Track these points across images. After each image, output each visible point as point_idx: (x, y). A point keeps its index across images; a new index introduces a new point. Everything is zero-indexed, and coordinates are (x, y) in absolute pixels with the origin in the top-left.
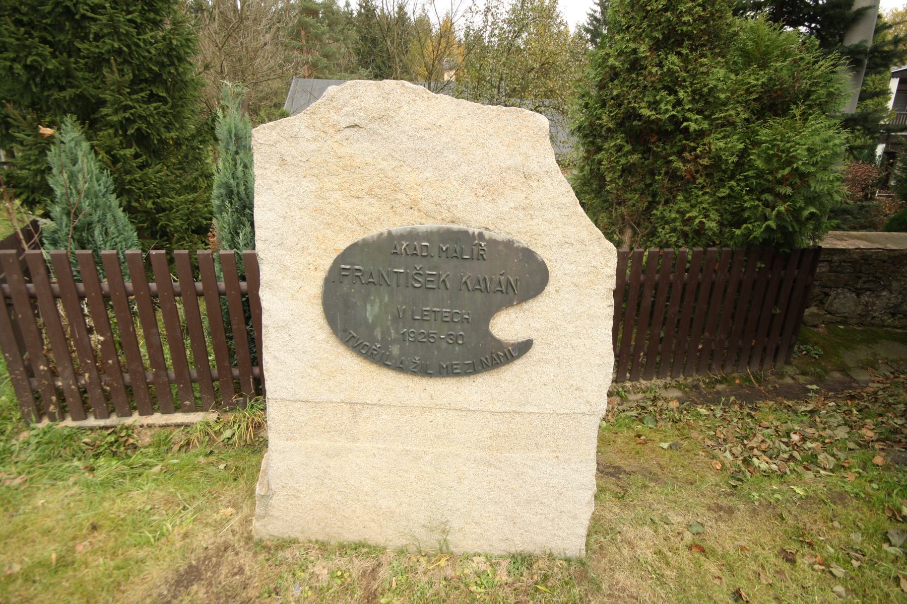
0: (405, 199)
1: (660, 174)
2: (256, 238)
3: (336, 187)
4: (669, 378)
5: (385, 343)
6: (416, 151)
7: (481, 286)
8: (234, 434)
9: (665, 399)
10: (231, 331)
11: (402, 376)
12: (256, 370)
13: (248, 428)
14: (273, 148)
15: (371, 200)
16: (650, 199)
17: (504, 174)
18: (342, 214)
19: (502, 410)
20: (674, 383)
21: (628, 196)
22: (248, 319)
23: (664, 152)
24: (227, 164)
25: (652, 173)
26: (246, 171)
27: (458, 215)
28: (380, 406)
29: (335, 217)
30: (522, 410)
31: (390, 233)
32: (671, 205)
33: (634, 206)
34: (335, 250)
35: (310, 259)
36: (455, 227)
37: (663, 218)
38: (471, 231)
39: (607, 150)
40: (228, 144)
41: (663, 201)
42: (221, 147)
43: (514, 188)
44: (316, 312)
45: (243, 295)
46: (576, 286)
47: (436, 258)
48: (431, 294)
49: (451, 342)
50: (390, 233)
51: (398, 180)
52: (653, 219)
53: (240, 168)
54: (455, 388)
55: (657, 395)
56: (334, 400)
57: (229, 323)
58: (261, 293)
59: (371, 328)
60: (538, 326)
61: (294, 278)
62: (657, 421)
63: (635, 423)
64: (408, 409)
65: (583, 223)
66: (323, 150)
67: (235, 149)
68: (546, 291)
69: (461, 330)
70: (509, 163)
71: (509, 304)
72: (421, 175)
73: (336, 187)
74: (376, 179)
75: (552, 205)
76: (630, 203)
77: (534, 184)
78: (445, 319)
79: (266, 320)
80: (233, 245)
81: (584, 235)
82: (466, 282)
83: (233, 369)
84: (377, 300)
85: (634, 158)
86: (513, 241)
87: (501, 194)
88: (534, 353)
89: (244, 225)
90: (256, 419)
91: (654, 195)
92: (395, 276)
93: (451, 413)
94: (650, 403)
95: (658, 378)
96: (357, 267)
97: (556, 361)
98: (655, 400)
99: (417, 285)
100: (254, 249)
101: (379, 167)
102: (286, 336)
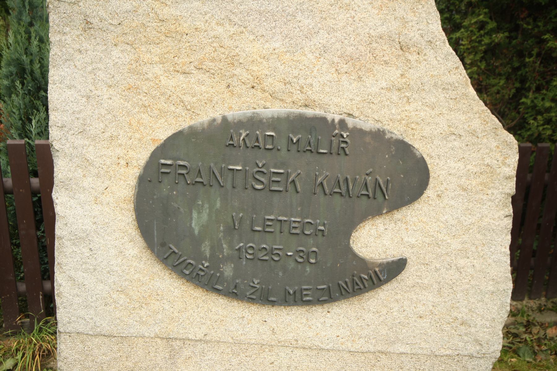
0: (245, 76)
1: (530, 56)
2: (50, 123)
3: (156, 59)
4: (543, 299)
5: (216, 261)
6: (260, 14)
7: (342, 189)
8: (16, 365)
9: (542, 325)
10: (18, 237)
11: (235, 303)
12: (47, 285)
13: (34, 357)
14: (76, 8)
15: (201, 76)
16: (518, 85)
17: (374, 45)
18: (162, 94)
19: (365, 349)
20: (550, 305)
21: (493, 81)
22: (39, 223)
23: (536, 30)
24: (19, 37)
25: (521, 55)
26: (43, 46)
27: (313, 97)
28: (206, 342)
29: (153, 97)
30: (391, 349)
31: (224, 119)
32: (544, 91)
33: (498, 93)
34: (154, 140)
35: (119, 151)
36: (309, 112)
37: (534, 107)
38: (329, 117)
39: (467, 28)
40: (20, 13)
41: (534, 87)
42: (12, 19)
43: (386, 63)
44: (126, 220)
45: (34, 193)
46: (465, 190)
47: (284, 152)
48: (276, 198)
49: (300, 260)
50: (224, 119)
51: (237, 51)
52: (522, 109)
53: (35, 43)
54: (304, 321)
55: (531, 318)
56: (147, 334)
57: (15, 227)
58: (54, 195)
59: (197, 241)
60: (413, 240)
61: (98, 176)
62: (535, 353)
63: (508, 356)
64: (243, 347)
65: (476, 109)
66: (140, 11)
67: (28, 19)
68: (425, 195)
69: (313, 246)
70: (382, 30)
71: (377, 212)
72: (267, 45)
73: (156, 59)
74: (208, 49)
75: (435, 85)
76: (495, 89)
77: (413, 57)
78: (294, 231)
79: (60, 230)
80: (24, 133)
81: (476, 124)
82: (321, 184)
83: (19, 284)
84: (207, 206)
85: (499, 37)
86: (384, 132)
87: (370, 70)
88: (407, 276)
89: (38, 110)
90: (45, 345)
91: (523, 81)
92: (230, 175)
93: (298, 352)
94: (522, 329)
95: (530, 298)
96: (181, 163)
97: (435, 286)
98: (528, 325)
99: (259, 187)
100: (48, 139)
101: (212, 34)
102: (87, 253)
